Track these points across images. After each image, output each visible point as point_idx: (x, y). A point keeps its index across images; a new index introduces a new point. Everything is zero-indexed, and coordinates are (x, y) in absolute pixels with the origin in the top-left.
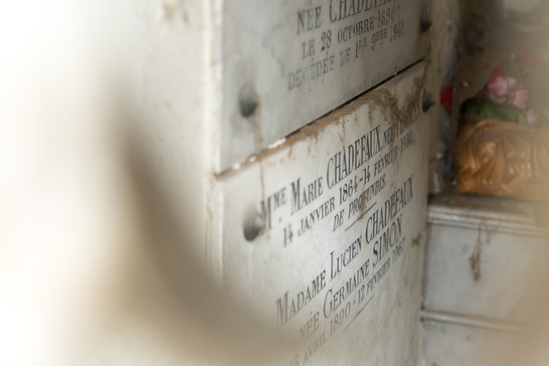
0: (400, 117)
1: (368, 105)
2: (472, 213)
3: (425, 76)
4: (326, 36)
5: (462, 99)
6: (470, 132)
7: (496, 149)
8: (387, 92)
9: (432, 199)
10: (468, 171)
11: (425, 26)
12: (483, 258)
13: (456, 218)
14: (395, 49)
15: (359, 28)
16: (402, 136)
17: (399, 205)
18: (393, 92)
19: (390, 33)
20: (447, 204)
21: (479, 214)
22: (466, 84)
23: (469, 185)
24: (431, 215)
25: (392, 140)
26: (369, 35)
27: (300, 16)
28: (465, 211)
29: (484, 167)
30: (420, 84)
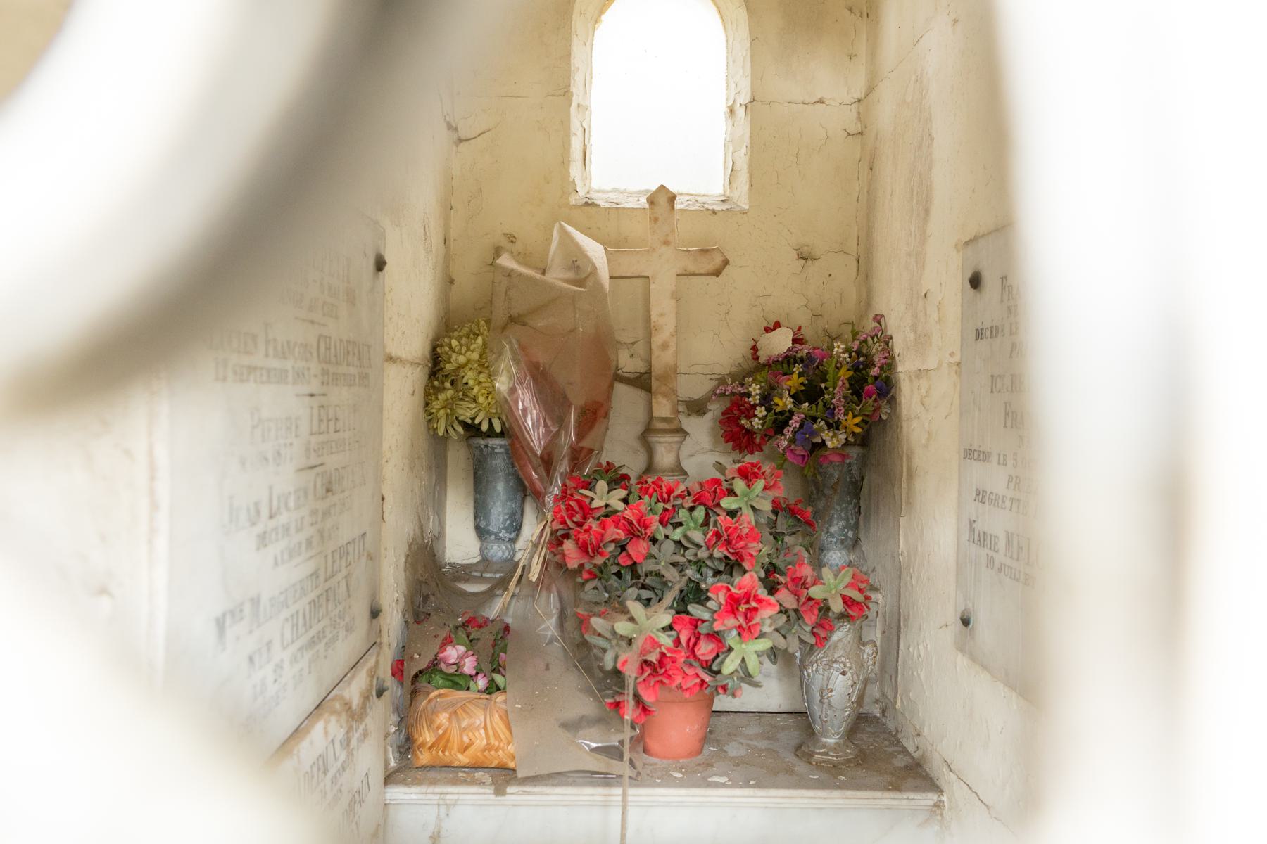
0: (355, 716)
1: (283, 402)
2: (431, 789)
3: (377, 662)
4: (279, 667)
5: (413, 673)
6: (423, 704)
7: (450, 719)
8: (342, 698)
9: (389, 779)
10: (422, 745)
11: (375, 613)
12: (443, 833)
13: (414, 796)
14: (346, 647)
15: (312, 643)
16: (357, 735)
17: (357, 807)
18: (346, 694)
19: (342, 633)
20: (404, 782)
21: (438, 789)
22: (416, 656)
23: (424, 758)
24: (388, 796)
25: (348, 745)
26: (321, 647)
27: (251, 659)
28: (423, 789)
29: (440, 738)
30: (372, 674)
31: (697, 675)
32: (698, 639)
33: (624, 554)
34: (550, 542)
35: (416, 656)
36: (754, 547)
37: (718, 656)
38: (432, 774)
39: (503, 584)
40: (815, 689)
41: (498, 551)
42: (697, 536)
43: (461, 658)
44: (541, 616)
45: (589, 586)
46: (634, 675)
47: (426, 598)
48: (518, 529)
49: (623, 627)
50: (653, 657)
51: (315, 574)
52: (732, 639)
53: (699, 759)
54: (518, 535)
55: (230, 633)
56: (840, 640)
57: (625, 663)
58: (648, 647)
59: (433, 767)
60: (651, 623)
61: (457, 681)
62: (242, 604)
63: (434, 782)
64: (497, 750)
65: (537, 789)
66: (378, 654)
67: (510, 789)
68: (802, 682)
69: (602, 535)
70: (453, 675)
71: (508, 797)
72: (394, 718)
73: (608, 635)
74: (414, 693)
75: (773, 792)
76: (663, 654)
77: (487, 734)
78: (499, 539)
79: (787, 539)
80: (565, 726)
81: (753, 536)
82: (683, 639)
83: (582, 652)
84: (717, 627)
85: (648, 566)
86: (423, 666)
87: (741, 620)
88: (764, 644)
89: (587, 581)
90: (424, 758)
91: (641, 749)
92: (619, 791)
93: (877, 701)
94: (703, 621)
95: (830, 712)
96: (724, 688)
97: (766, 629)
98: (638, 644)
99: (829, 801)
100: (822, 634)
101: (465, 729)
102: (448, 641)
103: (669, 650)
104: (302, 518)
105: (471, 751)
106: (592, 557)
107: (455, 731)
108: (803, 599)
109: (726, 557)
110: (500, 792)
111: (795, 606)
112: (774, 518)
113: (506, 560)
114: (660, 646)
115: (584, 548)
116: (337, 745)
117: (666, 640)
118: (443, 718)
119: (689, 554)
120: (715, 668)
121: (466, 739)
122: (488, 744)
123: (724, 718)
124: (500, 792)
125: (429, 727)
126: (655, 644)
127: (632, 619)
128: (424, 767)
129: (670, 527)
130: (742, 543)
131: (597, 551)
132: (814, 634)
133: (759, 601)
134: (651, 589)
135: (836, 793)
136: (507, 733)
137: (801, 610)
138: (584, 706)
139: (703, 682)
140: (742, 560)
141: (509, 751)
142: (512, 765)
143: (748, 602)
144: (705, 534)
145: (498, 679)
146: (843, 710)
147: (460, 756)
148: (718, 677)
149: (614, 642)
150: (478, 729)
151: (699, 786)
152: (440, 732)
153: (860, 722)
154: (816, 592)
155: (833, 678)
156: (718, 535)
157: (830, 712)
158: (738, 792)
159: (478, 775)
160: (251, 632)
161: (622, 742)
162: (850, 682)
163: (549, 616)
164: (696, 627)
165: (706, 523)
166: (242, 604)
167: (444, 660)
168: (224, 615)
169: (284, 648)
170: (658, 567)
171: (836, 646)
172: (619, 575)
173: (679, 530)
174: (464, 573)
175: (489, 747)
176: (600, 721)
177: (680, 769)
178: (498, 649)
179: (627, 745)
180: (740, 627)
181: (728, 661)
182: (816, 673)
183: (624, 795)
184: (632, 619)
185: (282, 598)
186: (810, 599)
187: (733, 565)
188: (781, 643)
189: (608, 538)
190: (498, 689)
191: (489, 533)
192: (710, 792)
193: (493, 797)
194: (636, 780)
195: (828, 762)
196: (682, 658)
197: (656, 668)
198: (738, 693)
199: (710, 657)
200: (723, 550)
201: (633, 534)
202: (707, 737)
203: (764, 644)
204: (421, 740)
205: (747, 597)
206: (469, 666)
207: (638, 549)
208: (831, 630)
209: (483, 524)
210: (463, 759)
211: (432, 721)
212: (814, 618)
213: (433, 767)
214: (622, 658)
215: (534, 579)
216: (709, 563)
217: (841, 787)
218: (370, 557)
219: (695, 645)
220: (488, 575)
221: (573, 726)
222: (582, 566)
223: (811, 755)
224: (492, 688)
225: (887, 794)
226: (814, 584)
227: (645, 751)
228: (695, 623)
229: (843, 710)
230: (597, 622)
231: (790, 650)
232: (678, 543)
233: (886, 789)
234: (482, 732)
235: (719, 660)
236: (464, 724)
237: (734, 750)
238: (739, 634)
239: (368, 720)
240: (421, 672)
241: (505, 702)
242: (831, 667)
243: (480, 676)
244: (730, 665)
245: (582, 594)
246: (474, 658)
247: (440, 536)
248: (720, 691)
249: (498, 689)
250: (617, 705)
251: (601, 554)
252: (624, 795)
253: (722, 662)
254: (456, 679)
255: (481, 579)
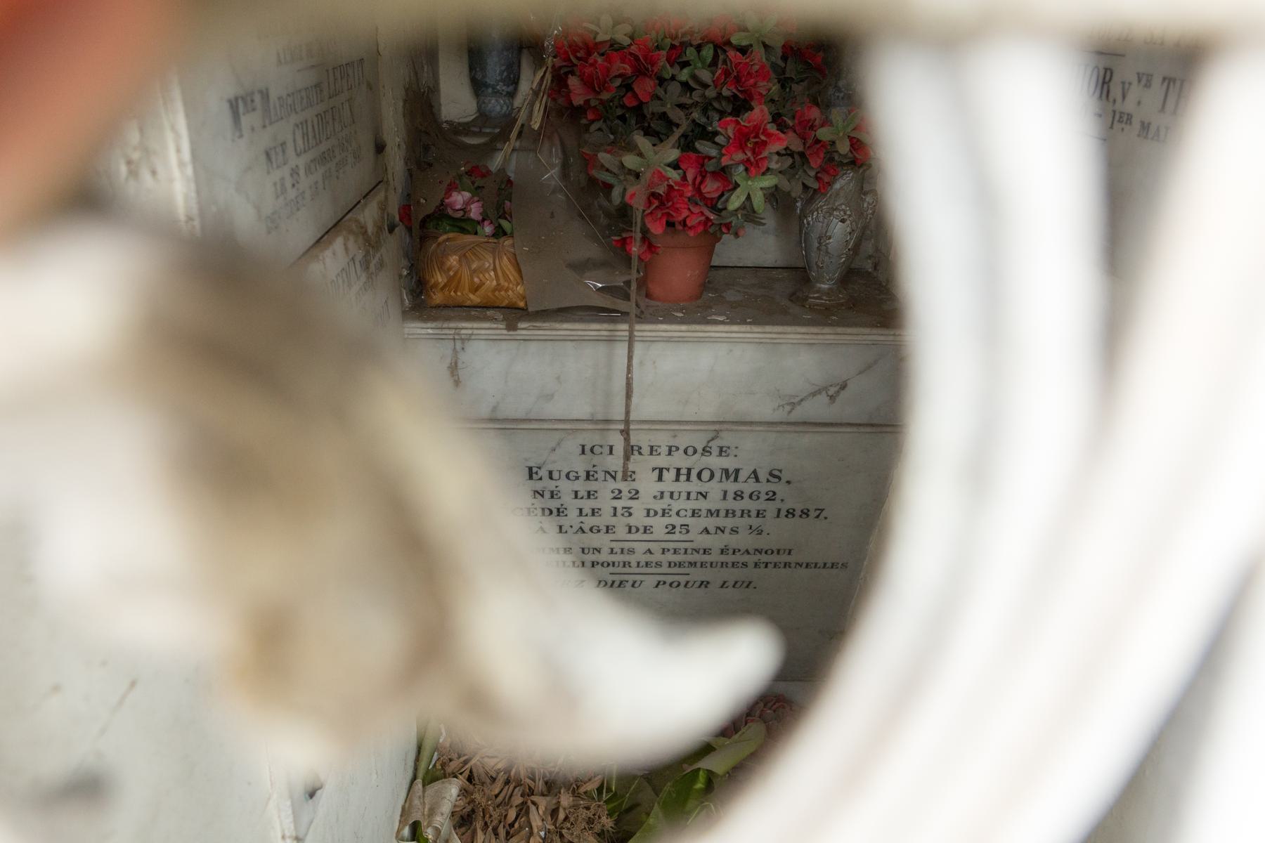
0: (371, 244)
3: (386, 198)
4: (294, 172)
5: (421, 217)
8: (357, 221)
11: (380, 148)
14: (356, 175)
21: (452, 325)
22: (423, 201)
23: (438, 298)
27: (268, 154)
29: (450, 279)
30: (383, 207)
31: (702, 214)
32: (704, 177)
33: (629, 94)
34: (551, 88)
35: (423, 201)
36: (763, 87)
37: (722, 195)
38: (445, 312)
39: (504, 136)
40: (814, 236)
41: (496, 106)
42: (705, 76)
43: (467, 203)
44: (545, 169)
45: (593, 127)
46: (641, 208)
47: (426, 148)
48: (515, 82)
49: (630, 161)
50: (661, 190)
51: (318, 86)
52: (738, 174)
53: (700, 302)
54: (516, 89)
55: (246, 120)
56: (842, 188)
57: (633, 195)
58: (656, 180)
59: (446, 307)
60: (657, 159)
61: (463, 225)
62: (253, 93)
63: (448, 319)
64: (507, 290)
65: (546, 325)
66: (386, 191)
67: (521, 325)
68: (801, 231)
69: (608, 70)
70: (460, 220)
71: (519, 332)
72: (405, 262)
73: (616, 170)
74: (424, 239)
75: (768, 328)
76: (670, 187)
77: (496, 275)
78: (496, 93)
79: (794, 86)
80: (573, 266)
81: (761, 74)
82: (690, 177)
83: (589, 189)
84: (725, 161)
85: (654, 107)
86: (430, 209)
87: (749, 154)
88: (768, 181)
89: (593, 121)
90: (438, 298)
91: (643, 292)
92: (625, 327)
93: (870, 257)
94: (710, 158)
95: (826, 259)
96: (728, 226)
97: (773, 166)
98: (647, 176)
99: (820, 337)
100: (826, 179)
101: (475, 271)
102: (452, 188)
103: (676, 183)
104: (283, 179)
105: (482, 291)
106: (598, 93)
107: (465, 273)
108: (810, 142)
109: (735, 96)
110: (511, 327)
111: (801, 149)
112: (783, 65)
113: (505, 116)
114: (668, 179)
115: (588, 83)
116: (357, 263)
117: (674, 175)
118: (453, 260)
119: (696, 96)
120: (720, 206)
121: (476, 280)
122: (498, 284)
123: (721, 272)
124: (511, 327)
125: (440, 269)
126: (663, 177)
127: (640, 155)
128: (438, 307)
129: (677, 67)
130: (752, 81)
131: (603, 86)
132: (817, 178)
133: (769, 135)
134: (658, 129)
135: (827, 330)
136: (516, 275)
137: (807, 153)
138: (591, 250)
139: (708, 218)
140: (752, 99)
141: (515, 292)
142: (522, 304)
143: (757, 136)
144: (713, 74)
145: (505, 224)
146: (839, 257)
147: (471, 296)
148: (724, 213)
149: (622, 177)
150: (487, 270)
151: (699, 323)
152: (451, 273)
153: (850, 275)
154: (824, 134)
155: (832, 225)
156: (727, 73)
157: (826, 259)
158: (735, 328)
159: (489, 313)
160: (264, 127)
161: (628, 283)
162: (849, 230)
163: (553, 166)
164: (703, 165)
165: (714, 63)
166: (253, 93)
167: (451, 205)
168: (236, 99)
169: (298, 155)
170: (663, 109)
171: (838, 194)
172: (622, 118)
173: (686, 71)
174: (465, 129)
175: (499, 288)
176: (604, 264)
177: (681, 310)
178: (503, 201)
179: (634, 286)
180: (748, 160)
181: (733, 197)
182: (816, 220)
183: (631, 331)
184: (640, 155)
185: (290, 101)
186: (817, 141)
187: (740, 105)
188: (785, 185)
189: (614, 73)
190: (505, 234)
191: (486, 86)
192: (709, 328)
193: (505, 332)
194: (641, 318)
195: (821, 305)
196: (689, 192)
197: (661, 201)
198: (741, 233)
199: (716, 195)
200: (732, 88)
201: (640, 72)
202: (705, 286)
203: (768, 181)
204: (433, 281)
205: (756, 130)
206: (475, 211)
207: (645, 87)
208: (835, 177)
209: (479, 76)
210: (475, 299)
211: (443, 263)
212: (819, 161)
213: (446, 307)
214: (630, 191)
215: (536, 127)
216: (716, 105)
217: (838, 324)
218: (370, 87)
219: (701, 183)
220: (488, 130)
221: (581, 267)
222: (587, 102)
223: (807, 298)
224: (499, 233)
225: (875, 331)
226: (822, 126)
227: (648, 296)
228: (702, 159)
229: (839, 257)
230: (604, 157)
231: (793, 195)
232: (685, 85)
233: (873, 326)
234: (492, 273)
235: (723, 199)
236: (474, 266)
237: (731, 295)
238: (746, 170)
239: (383, 250)
240: (428, 216)
241: (513, 246)
242: (831, 214)
243: (486, 223)
244: (735, 201)
245: (587, 136)
246: (480, 204)
247: (434, 89)
248: (724, 230)
249: (505, 234)
250: (624, 242)
251: (608, 90)
252: (631, 331)
253: (727, 201)
254: (463, 225)
255: (480, 134)
